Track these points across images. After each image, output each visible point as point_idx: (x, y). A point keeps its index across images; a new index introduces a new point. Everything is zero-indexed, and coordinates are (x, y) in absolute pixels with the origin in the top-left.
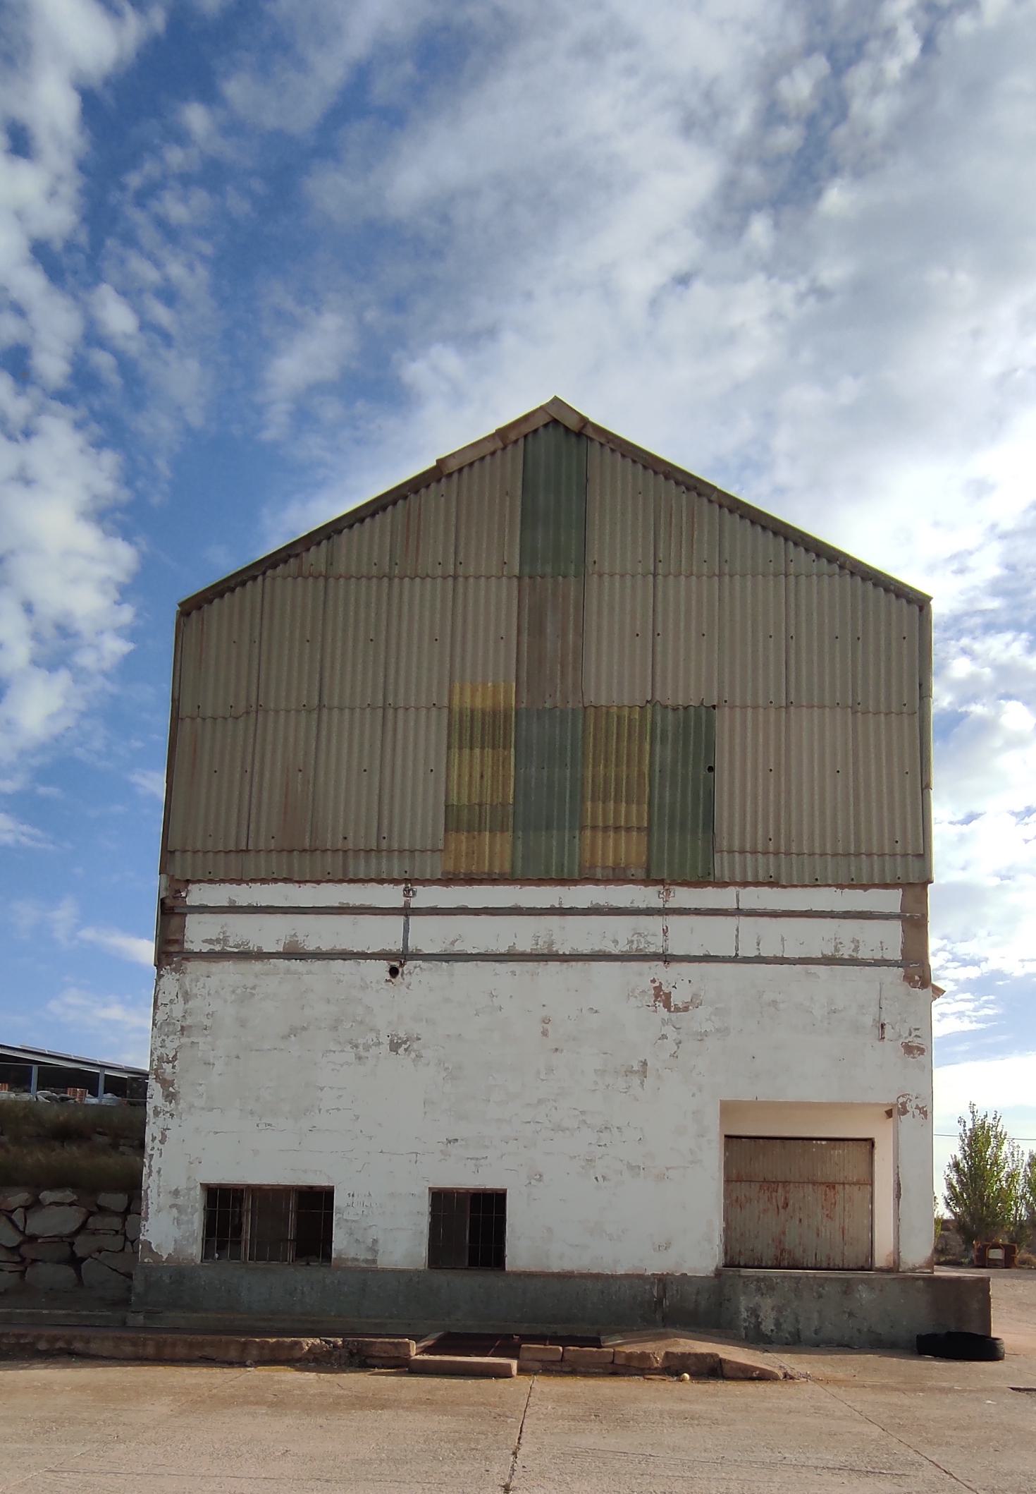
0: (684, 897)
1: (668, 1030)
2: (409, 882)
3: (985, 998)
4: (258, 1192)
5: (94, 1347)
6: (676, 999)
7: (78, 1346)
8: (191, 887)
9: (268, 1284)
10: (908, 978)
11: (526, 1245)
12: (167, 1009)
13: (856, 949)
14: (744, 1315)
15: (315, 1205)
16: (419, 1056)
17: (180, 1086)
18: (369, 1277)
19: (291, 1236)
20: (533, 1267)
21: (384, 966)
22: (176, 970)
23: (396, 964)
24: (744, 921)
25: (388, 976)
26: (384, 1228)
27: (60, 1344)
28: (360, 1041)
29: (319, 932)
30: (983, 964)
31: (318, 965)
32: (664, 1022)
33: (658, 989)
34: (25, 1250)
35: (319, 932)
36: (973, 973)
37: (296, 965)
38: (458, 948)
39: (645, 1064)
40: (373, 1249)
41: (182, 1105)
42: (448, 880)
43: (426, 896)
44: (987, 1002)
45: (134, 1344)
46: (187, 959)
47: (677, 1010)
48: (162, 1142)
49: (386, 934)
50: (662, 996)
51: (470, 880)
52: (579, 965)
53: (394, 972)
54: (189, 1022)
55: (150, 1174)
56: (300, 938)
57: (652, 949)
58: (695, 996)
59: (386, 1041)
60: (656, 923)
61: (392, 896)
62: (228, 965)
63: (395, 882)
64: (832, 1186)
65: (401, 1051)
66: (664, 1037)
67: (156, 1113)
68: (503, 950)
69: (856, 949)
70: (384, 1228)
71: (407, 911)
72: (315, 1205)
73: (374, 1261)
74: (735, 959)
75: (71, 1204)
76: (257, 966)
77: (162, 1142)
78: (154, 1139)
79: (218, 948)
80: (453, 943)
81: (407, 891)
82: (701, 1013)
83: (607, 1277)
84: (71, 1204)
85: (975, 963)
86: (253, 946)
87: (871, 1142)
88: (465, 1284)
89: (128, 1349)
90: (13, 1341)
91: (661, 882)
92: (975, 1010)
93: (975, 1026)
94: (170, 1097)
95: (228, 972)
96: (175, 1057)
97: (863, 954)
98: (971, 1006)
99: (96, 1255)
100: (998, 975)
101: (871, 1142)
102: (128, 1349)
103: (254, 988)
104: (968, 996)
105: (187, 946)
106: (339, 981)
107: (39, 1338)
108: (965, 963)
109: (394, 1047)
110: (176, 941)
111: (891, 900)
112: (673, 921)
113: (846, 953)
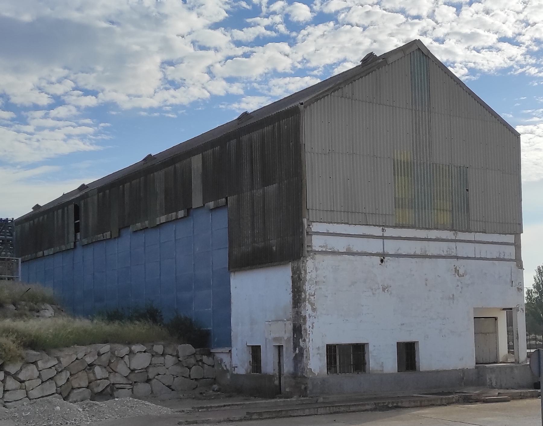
0: (461, 236)
1: (459, 283)
2: (384, 226)
3: (102, 125)
4: (340, 346)
5: (404, 404)
6: (461, 272)
7: (400, 404)
8: (313, 224)
9: (349, 382)
10: (517, 265)
11: (426, 361)
12: (310, 274)
13: (504, 256)
14: (488, 381)
15: (359, 350)
16: (391, 293)
17: (317, 306)
18: (383, 377)
19: (352, 363)
20: (428, 370)
21: (378, 259)
22: (312, 258)
23: (382, 258)
24: (477, 245)
25: (380, 263)
26: (383, 359)
27: (395, 405)
28: (374, 287)
29: (358, 245)
30: (101, 95)
31: (358, 258)
32: (458, 280)
33: (456, 268)
34: (132, 376)
35: (358, 245)
36: (90, 101)
37: (351, 257)
38: (400, 252)
39: (453, 295)
40: (382, 366)
41: (318, 313)
42: (395, 227)
43: (389, 232)
44: (105, 128)
45: (414, 402)
46: (315, 254)
47: (461, 276)
48: (312, 328)
49: (375, 246)
50: (457, 271)
51: (403, 227)
52: (366, 239)
53: (382, 261)
54: (318, 279)
55: (309, 342)
56: (351, 247)
57: (453, 254)
58: (465, 271)
59: (381, 287)
60: (453, 245)
61: (377, 231)
62: (329, 257)
63: (379, 226)
64: (486, 334)
65: (386, 291)
66: (458, 286)
67: (310, 317)
68: (412, 253)
69: (504, 256)
70: (383, 359)
71: (383, 238)
72: (359, 350)
73: (383, 371)
74: (475, 258)
75: (145, 352)
76: (339, 257)
77: (312, 328)
78: (310, 327)
79: (324, 250)
80: (398, 250)
81: (383, 229)
82: (467, 277)
83: (449, 371)
84: (145, 352)
85: (94, 93)
86: (336, 250)
87: (496, 319)
88: (408, 376)
89: (413, 404)
90: (382, 404)
91: (455, 230)
92: (95, 134)
93: (92, 148)
94: (314, 310)
95: (329, 260)
96: (314, 294)
97: (506, 257)
98: (91, 130)
99: (156, 377)
100: (112, 105)
101: (496, 319)
102: (413, 404)
103: (339, 266)
104: (88, 121)
105: (314, 248)
106: (365, 264)
107: (389, 403)
108: (87, 93)
109: (384, 290)
110: (310, 246)
111: (510, 238)
112: (458, 244)
113: (502, 257)
